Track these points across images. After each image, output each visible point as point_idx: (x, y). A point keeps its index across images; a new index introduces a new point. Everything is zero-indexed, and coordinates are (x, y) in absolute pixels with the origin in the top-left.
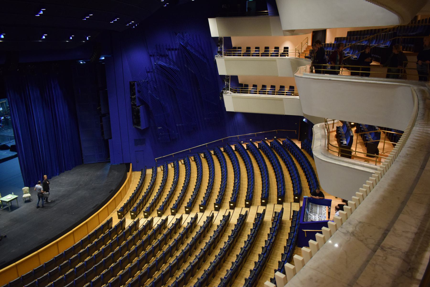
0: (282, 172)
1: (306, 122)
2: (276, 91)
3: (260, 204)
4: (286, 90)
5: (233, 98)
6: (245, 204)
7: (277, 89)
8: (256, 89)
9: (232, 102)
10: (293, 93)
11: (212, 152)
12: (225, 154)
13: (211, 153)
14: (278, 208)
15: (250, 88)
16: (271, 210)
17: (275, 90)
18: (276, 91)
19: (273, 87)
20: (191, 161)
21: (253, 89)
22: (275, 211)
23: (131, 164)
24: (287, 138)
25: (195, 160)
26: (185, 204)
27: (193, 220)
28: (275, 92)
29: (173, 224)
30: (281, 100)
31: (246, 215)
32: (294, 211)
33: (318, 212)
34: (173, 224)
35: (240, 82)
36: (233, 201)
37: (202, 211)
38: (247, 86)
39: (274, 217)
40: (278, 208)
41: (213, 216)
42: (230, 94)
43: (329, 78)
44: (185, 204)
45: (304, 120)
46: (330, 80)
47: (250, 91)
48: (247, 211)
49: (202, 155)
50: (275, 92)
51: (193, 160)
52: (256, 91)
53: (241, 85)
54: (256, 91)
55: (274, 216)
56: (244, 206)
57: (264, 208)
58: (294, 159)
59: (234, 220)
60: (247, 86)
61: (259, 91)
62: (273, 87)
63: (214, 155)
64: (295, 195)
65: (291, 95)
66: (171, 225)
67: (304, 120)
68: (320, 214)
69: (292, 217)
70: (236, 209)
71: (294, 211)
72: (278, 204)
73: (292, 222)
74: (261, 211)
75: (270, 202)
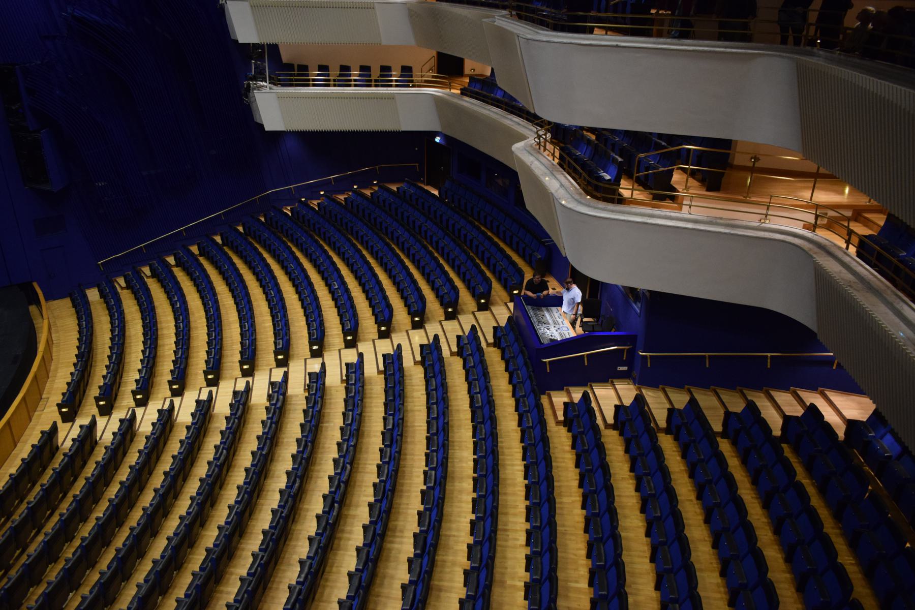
0: (313, 291)
1: (443, 143)
2: (373, 78)
3: (274, 364)
4: (355, 75)
5: (280, 97)
6: (242, 370)
7: (375, 74)
8: (328, 75)
9: (276, 108)
10: (412, 81)
11: (171, 260)
12: (201, 259)
13: (168, 266)
14: (351, 356)
15: (314, 73)
16: (373, 352)
17: (370, 76)
18: (373, 78)
19: (365, 69)
20: (119, 290)
21: (319, 75)
22: (308, 371)
23: (35, 285)
24: (408, 182)
25: (129, 286)
26: (94, 391)
27: (126, 424)
28: (371, 81)
29: (73, 440)
30: (391, 97)
31: (248, 390)
32: (347, 365)
33: (550, 321)
34: (73, 440)
35: (285, 58)
36: (212, 368)
37: (142, 403)
38: (304, 68)
39: (308, 386)
40: (419, 338)
41: (134, 416)
42: (270, 88)
43: (615, 43)
44: (94, 391)
45: (438, 139)
46: (617, 46)
47: (314, 80)
48: (248, 382)
49: (121, 281)
50: (371, 81)
51: (123, 284)
52: (329, 80)
53: (290, 67)
54: (329, 80)
55: (308, 382)
56: (239, 373)
57: (320, 360)
58: (336, 259)
59: (222, 406)
60: (304, 68)
61: (334, 80)
62: (365, 69)
63: (177, 265)
64: (345, 333)
65: (408, 86)
66: (68, 443)
67: (438, 139)
68: (555, 324)
69: (344, 378)
70: (222, 384)
71: (347, 365)
72: (446, 319)
73: (347, 389)
74: (241, 386)
75: (428, 319)
